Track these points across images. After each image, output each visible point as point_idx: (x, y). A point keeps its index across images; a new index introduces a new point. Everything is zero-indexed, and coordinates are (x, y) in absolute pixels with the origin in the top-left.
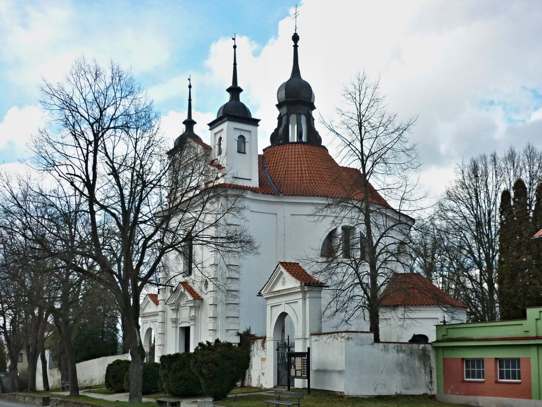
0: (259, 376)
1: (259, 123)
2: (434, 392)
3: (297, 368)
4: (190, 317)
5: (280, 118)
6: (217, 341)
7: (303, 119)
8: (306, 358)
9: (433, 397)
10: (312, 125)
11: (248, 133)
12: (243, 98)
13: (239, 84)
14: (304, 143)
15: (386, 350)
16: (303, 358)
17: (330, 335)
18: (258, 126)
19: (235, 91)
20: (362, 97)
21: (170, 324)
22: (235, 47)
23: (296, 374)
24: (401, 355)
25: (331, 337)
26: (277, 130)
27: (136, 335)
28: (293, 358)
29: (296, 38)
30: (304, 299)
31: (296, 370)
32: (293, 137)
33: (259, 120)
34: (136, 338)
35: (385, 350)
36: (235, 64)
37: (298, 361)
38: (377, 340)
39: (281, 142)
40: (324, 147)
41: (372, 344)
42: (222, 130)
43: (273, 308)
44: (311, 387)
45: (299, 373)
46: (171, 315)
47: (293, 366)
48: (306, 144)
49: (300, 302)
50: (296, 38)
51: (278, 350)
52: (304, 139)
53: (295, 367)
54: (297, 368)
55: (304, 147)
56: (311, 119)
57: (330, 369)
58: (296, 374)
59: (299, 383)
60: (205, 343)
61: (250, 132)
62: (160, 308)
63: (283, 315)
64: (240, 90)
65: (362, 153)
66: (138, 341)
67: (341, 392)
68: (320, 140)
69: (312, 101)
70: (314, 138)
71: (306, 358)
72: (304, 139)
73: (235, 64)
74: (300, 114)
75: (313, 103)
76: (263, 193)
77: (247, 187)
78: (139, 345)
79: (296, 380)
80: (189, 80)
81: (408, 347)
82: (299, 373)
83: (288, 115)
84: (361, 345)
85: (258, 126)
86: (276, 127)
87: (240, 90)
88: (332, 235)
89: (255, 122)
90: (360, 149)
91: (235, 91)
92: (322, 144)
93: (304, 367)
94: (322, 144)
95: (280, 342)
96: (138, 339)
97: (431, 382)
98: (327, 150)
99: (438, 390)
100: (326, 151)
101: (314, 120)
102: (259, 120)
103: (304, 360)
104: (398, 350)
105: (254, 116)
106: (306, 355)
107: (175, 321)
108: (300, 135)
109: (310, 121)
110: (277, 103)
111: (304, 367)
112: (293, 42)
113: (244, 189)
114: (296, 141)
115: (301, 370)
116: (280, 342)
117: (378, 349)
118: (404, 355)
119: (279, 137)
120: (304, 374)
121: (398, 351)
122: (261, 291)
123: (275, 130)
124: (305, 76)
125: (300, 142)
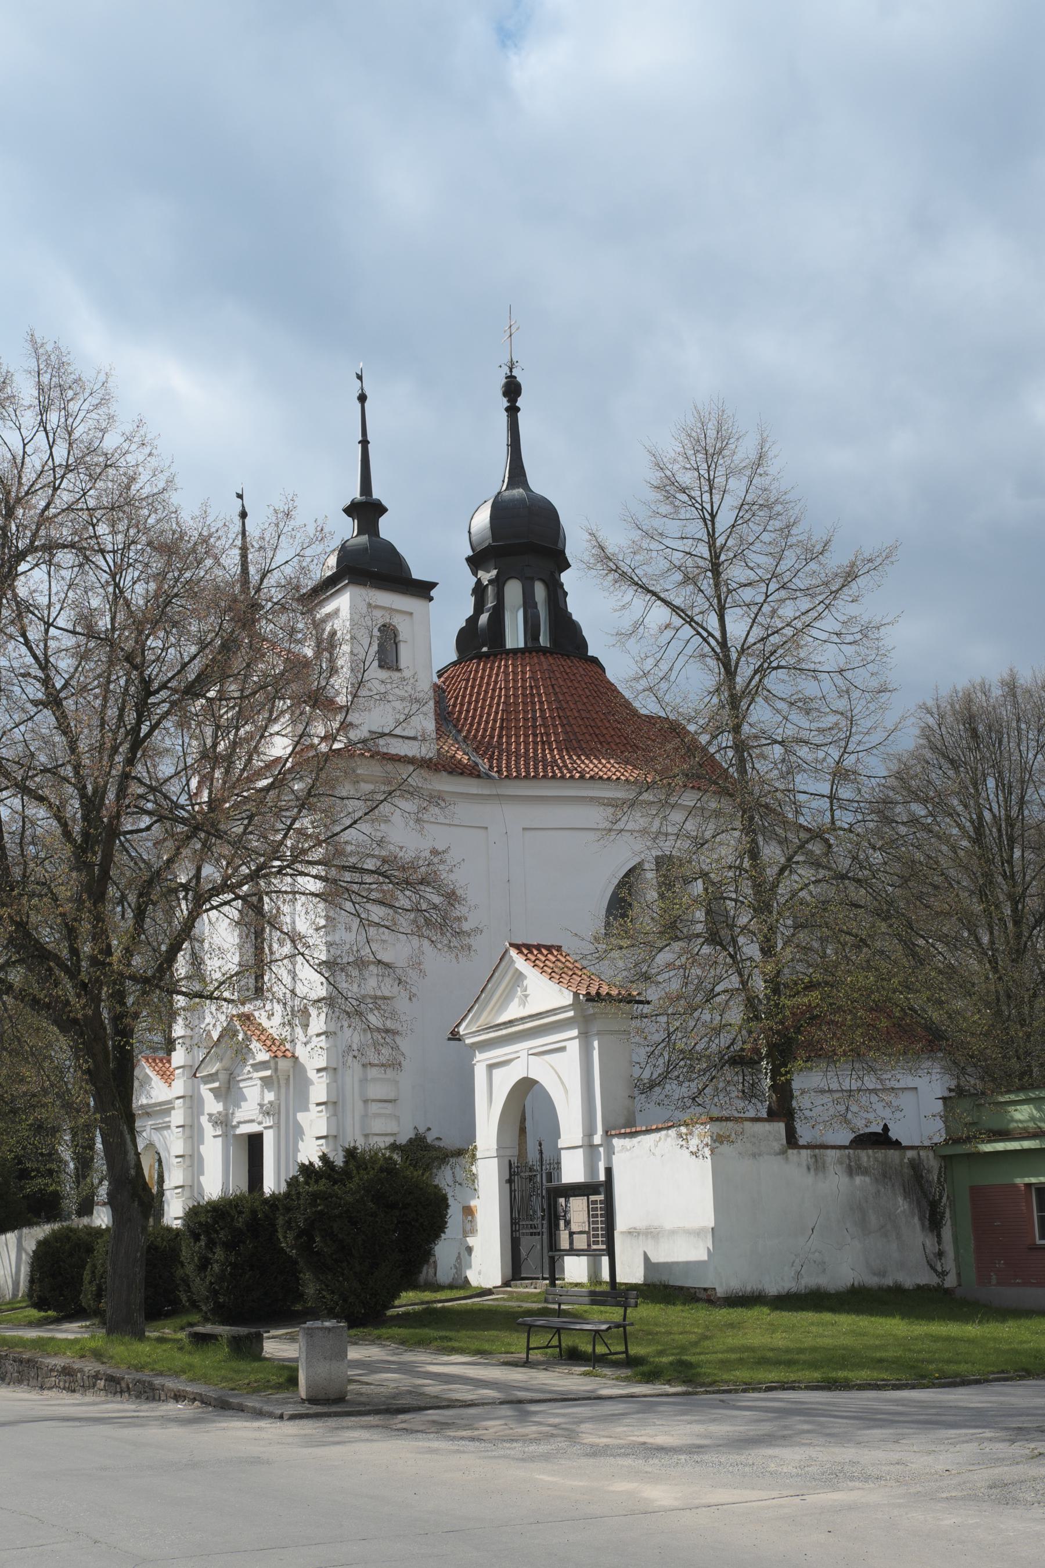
0: (459, 1257)
1: (433, 593)
2: (950, 1282)
3: (574, 1228)
4: (261, 1105)
5: (479, 591)
6: (351, 1154)
7: (540, 591)
8: (601, 1197)
9: (948, 1292)
10: (562, 606)
11: (407, 618)
12: (388, 528)
13: (377, 494)
14: (544, 651)
15: (818, 1166)
16: (592, 1198)
17: (664, 1133)
18: (431, 599)
19: (366, 511)
20: (716, 498)
21: (209, 1130)
22: (362, 398)
23: (571, 1243)
24: (858, 1180)
25: (667, 1136)
26: (472, 621)
27: (123, 1143)
28: (562, 1200)
29: (512, 389)
30: (585, 1037)
31: (571, 1234)
32: (515, 636)
33: (433, 585)
34: (126, 1153)
35: (816, 1169)
36: (364, 443)
37: (578, 1210)
38: (792, 1140)
39: (485, 649)
40: (595, 661)
41: (783, 1152)
42: (337, 612)
43: (495, 1072)
44: (619, 1279)
45: (580, 1242)
46: (213, 1105)
47: (562, 1223)
48: (551, 654)
49: (574, 1048)
50: (512, 389)
51: (510, 1181)
52: (544, 640)
53: (568, 1223)
54: (574, 1228)
55: (545, 662)
56: (559, 591)
57: (668, 1226)
58: (571, 1243)
59: (575, 1270)
60: (318, 1163)
61: (411, 614)
62: (179, 1087)
63: (526, 1087)
64: (379, 509)
65: (723, 644)
66: (132, 1163)
67: (705, 1289)
68: (584, 645)
69: (560, 545)
70: (567, 638)
71: (601, 1197)
72: (544, 640)
73: (364, 443)
74: (532, 580)
75: (562, 552)
76: (450, 773)
77: (406, 756)
78: (133, 1172)
79: (568, 1260)
80: (240, 496)
81: (876, 1159)
82: (580, 1242)
83: (499, 583)
84: (754, 1155)
85: (431, 599)
86: (470, 612)
87: (379, 509)
88: (630, 879)
89: (423, 590)
90: (718, 634)
91: (366, 511)
92: (590, 654)
93: (596, 1216)
94: (590, 654)
95: (514, 1160)
96: (131, 1156)
97: (940, 1254)
98: (603, 669)
99: (959, 1275)
100: (601, 672)
101: (566, 594)
102: (433, 585)
103: (595, 1202)
104: (849, 1167)
105: (416, 575)
106: (600, 1191)
107: (223, 1122)
108: (532, 629)
109: (557, 595)
110: (471, 553)
111: (595, 1222)
112: (505, 400)
113: (399, 760)
114: (522, 645)
115: (587, 1233)
116: (514, 1160)
117: (799, 1165)
118: (867, 1179)
119: (478, 641)
120: (596, 1243)
121: (851, 1172)
122: (458, 1026)
123: (467, 620)
124: (540, 483)
125: (532, 648)
